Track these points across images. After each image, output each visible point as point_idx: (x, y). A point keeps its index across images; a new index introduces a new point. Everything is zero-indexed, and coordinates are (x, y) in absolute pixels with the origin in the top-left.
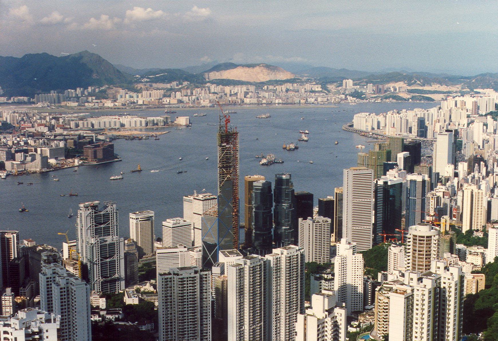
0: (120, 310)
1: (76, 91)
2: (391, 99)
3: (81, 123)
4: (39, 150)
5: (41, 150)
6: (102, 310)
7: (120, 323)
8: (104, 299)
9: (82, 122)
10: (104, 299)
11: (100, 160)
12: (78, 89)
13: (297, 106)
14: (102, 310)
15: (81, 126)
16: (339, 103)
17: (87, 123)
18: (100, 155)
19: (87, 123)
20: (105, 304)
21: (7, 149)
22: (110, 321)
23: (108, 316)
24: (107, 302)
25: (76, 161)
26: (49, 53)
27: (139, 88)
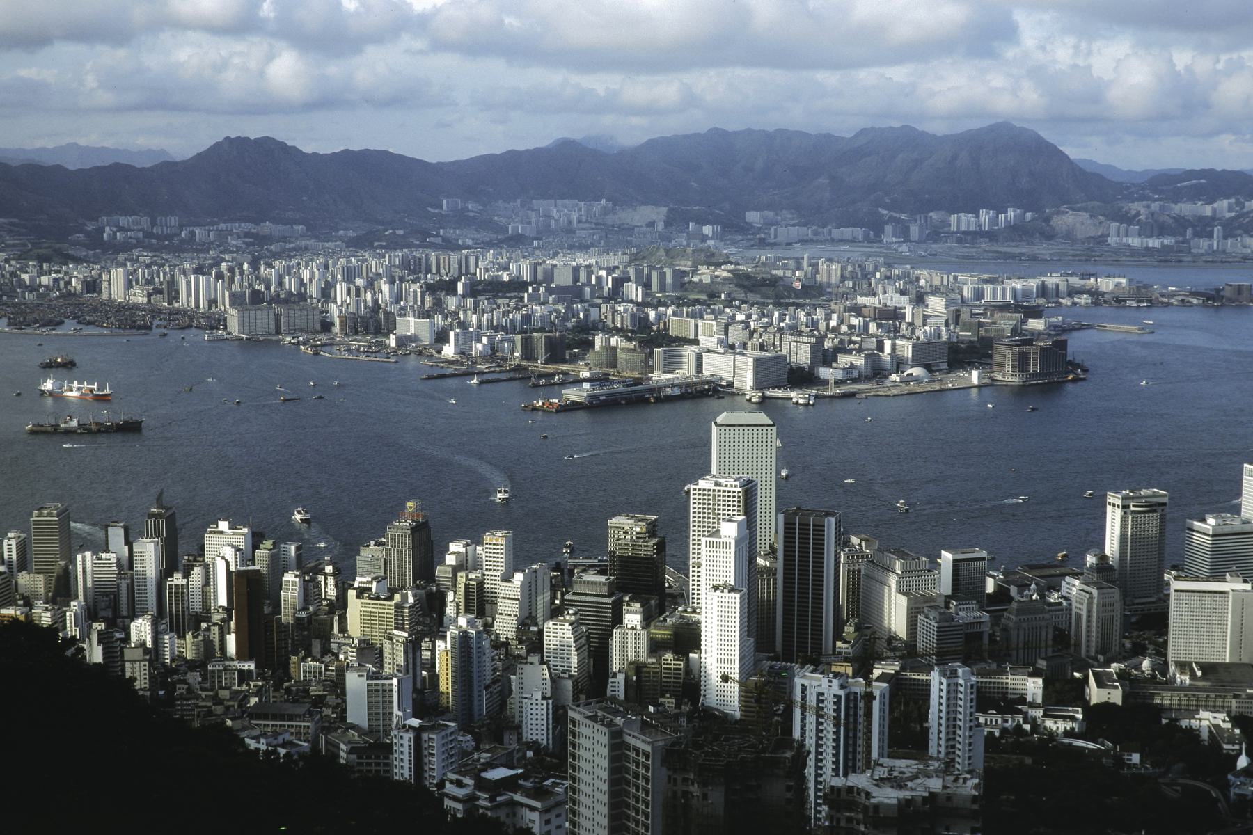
0: (1077, 712)
1: (978, 216)
2: (797, 278)
3: (988, 288)
4: (888, 344)
5: (894, 346)
6: (1033, 705)
7: (1077, 743)
8: (1040, 681)
9: (990, 286)
10: (1040, 681)
11: (1035, 375)
12: (983, 212)
13: (986, 276)
14: (1033, 705)
15: (988, 297)
16: (744, 302)
17: (1004, 290)
18: (1034, 365)
19: (1004, 290)
20: (1040, 692)
21: (813, 340)
22: (1052, 735)
23: (1049, 723)
24: (1045, 688)
25: (975, 374)
26: (1119, 166)
27: (1133, 212)
